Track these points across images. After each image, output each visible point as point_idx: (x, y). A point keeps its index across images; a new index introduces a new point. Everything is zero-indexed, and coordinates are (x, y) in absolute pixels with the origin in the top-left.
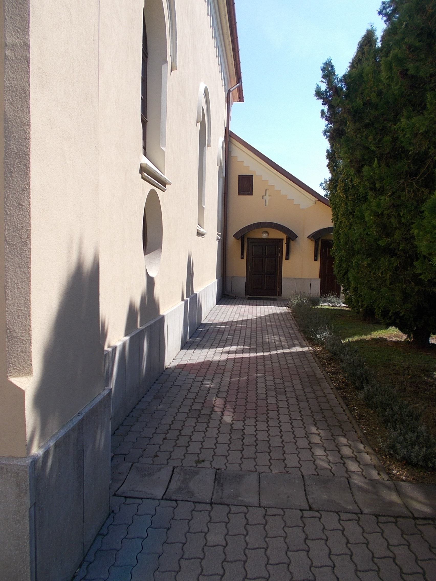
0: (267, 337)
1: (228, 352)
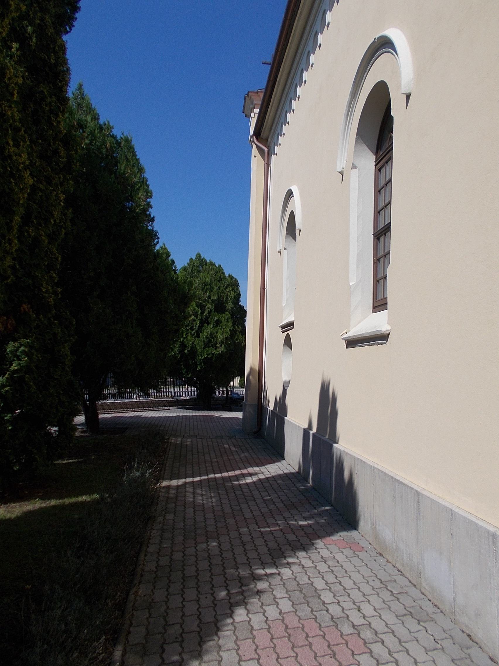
0: (214, 500)
1: (251, 475)
